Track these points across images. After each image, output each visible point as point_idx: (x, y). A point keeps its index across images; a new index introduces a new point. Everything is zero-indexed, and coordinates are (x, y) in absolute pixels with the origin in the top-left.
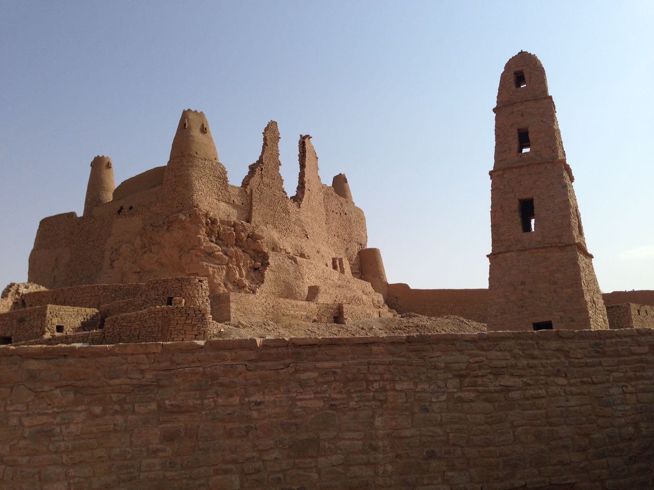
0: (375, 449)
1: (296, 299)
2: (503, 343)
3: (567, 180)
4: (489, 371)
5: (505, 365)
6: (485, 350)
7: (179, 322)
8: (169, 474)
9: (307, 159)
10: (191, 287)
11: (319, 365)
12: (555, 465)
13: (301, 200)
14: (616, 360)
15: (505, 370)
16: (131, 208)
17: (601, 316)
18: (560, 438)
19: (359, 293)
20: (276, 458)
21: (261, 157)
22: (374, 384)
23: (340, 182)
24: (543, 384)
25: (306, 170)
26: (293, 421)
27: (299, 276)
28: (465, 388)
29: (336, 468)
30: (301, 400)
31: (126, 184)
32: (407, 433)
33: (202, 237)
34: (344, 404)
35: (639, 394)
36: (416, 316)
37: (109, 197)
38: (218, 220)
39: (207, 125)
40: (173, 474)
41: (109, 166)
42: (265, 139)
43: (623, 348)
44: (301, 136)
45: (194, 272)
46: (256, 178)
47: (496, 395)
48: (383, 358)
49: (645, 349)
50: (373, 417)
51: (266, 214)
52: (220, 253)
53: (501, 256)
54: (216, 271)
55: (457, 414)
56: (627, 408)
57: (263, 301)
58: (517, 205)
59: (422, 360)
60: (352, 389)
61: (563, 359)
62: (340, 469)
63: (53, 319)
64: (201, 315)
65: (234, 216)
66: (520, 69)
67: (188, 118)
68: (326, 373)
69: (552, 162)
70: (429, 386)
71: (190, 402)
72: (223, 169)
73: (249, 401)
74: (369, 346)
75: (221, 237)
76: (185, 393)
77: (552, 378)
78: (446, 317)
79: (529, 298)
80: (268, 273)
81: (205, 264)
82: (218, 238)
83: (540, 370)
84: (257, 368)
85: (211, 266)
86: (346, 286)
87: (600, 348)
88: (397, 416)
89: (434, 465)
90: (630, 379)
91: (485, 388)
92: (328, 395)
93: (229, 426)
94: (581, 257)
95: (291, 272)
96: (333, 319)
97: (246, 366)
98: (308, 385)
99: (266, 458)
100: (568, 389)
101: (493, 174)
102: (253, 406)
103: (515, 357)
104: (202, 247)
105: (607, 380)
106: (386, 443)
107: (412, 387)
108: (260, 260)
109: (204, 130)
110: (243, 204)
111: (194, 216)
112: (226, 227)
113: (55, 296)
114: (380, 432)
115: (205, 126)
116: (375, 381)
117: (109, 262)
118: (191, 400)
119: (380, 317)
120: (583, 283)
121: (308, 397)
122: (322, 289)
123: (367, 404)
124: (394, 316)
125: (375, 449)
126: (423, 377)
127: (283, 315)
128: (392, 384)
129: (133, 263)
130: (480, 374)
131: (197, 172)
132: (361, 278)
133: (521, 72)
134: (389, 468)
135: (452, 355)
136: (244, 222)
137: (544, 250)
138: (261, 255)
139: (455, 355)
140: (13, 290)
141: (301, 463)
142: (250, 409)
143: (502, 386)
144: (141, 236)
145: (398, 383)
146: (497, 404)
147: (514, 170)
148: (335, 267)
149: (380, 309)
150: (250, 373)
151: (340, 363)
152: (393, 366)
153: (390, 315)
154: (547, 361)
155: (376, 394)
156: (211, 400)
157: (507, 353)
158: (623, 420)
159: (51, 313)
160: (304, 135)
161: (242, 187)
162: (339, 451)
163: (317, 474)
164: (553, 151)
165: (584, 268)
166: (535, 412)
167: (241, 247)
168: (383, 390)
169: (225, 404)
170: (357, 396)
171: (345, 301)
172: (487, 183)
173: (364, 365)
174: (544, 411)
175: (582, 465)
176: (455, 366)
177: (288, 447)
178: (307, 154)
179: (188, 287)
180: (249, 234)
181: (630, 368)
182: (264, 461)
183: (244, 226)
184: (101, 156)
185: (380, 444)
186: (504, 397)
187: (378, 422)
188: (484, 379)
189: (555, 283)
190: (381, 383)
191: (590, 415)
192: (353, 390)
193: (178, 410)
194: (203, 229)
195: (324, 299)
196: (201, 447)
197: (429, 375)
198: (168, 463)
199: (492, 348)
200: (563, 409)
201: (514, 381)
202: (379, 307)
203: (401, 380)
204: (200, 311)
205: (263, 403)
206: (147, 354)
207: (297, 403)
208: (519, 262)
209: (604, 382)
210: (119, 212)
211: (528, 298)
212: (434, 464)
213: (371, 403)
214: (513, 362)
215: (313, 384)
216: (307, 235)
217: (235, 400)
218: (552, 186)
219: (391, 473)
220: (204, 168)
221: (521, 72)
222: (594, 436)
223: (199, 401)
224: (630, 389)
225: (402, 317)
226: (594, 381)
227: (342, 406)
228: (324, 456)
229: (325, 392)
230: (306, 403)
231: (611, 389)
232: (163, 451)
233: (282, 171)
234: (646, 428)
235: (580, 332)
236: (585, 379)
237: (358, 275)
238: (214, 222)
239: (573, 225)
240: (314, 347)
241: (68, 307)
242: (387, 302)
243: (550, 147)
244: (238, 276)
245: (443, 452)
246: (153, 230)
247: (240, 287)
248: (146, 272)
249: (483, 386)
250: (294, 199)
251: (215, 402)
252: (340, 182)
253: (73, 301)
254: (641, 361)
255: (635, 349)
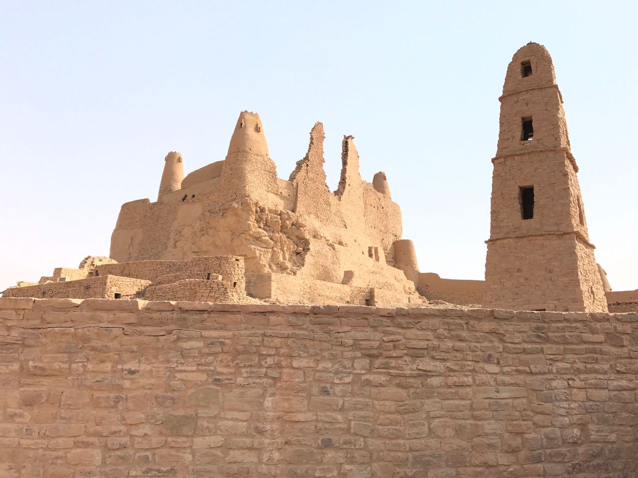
0: (261, 432)
1: (332, 281)
2: (426, 321)
3: (570, 168)
4: (405, 352)
5: (426, 347)
6: (403, 328)
7: (204, 294)
8: (25, 442)
9: (349, 157)
10: (228, 265)
11: (205, 333)
12: (477, 466)
13: (342, 194)
14: (562, 347)
15: (425, 352)
16: (194, 196)
17: (600, 307)
18: (486, 435)
19: (392, 281)
20: (145, 435)
21: (307, 154)
22: (268, 358)
23: (379, 181)
24: (470, 371)
25: (347, 167)
26: (169, 394)
27: (336, 261)
28: (375, 370)
29: (213, 451)
30: (181, 371)
31: (191, 176)
32: (301, 417)
33: (252, 223)
34: (231, 380)
35: (589, 390)
36: (444, 303)
37: (178, 186)
38: (267, 209)
39: (261, 124)
40: (29, 442)
41: (179, 160)
42: (312, 138)
43: (571, 334)
44: (345, 136)
45: (243, 254)
46: (302, 172)
47: (412, 380)
48: (281, 330)
49: (601, 338)
50: (263, 396)
51: (309, 205)
52: (267, 238)
53: (498, 242)
54: (262, 253)
55: (362, 400)
56: (572, 406)
57: (301, 282)
58: (518, 192)
59: (326, 335)
60: (241, 363)
61: (496, 344)
62: (218, 453)
63: (112, 287)
64: (223, 289)
65: (281, 206)
66: (527, 59)
67: (244, 118)
68: (212, 344)
69: (554, 150)
70: (333, 364)
71: (56, 366)
72: (273, 164)
73: (122, 369)
74: (267, 315)
75: (268, 224)
76: (51, 355)
77: (481, 364)
78: (471, 305)
79: (524, 285)
80: (308, 258)
81: (253, 247)
82: (266, 225)
83: (467, 355)
84: (135, 333)
85: (258, 249)
86: (379, 272)
87: (542, 333)
88: (291, 397)
89: (330, 455)
90: (578, 371)
91: (399, 372)
92: (213, 368)
93: (97, 394)
94: (580, 248)
95: (329, 257)
96: (364, 302)
97: (124, 329)
98: (191, 355)
99: (134, 433)
100: (500, 378)
101: (496, 161)
102: (125, 375)
103: (438, 338)
104: (251, 232)
105: (549, 371)
106: (275, 426)
107: (312, 365)
108: (302, 246)
109: (258, 129)
110: (289, 195)
111: (246, 205)
112: (273, 215)
113: (122, 269)
114: (268, 413)
115: (259, 126)
116: (270, 355)
117: (174, 242)
118: (57, 363)
119: (409, 302)
120: (579, 273)
121: (189, 368)
122: (356, 274)
123: (258, 381)
124: (424, 302)
125: (261, 432)
126: (326, 354)
127: (319, 295)
128: (289, 361)
129: (192, 244)
130: (394, 355)
131: (250, 166)
132: (394, 266)
133: (529, 62)
134: (276, 455)
135: (363, 331)
136: (289, 212)
137: (542, 238)
138: (302, 241)
139: (367, 332)
140: (89, 262)
141: (173, 441)
142: (122, 377)
143: (419, 370)
144: (201, 221)
145: (295, 359)
146: (412, 390)
147: (516, 158)
148: (370, 255)
149: (410, 295)
150: (127, 338)
151: (231, 333)
152: (292, 339)
153: (420, 301)
154: (476, 344)
155: (269, 371)
156: (81, 364)
157: (429, 333)
158: (566, 419)
159: (110, 282)
160: (347, 135)
161: (289, 180)
162: (219, 432)
163: (191, 456)
164: (556, 139)
165: (582, 257)
166: (457, 402)
167: (286, 233)
168: (278, 366)
169: (95, 370)
170: (247, 372)
171: (377, 286)
172: (489, 169)
173: (258, 337)
174: (468, 402)
175: (511, 469)
176: (364, 344)
177: (160, 422)
178: (349, 153)
179: (226, 265)
180: (293, 222)
181: (579, 359)
182: (131, 436)
183: (290, 215)
184: (173, 152)
185: (268, 427)
186: (422, 383)
187: (268, 402)
188: (399, 362)
189: (551, 271)
190: (276, 358)
191: (525, 410)
192: (242, 365)
193: (42, 373)
194: (253, 216)
195: (358, 282)
196: (63, 415)
197: (334, 352)
198: (24, 430)
199: (412, 326)
200: (492, 401)
201: (434, 366)
202: (410, 293)
203: (299, 356)
204: (223, 285)
205: (138, 371)
206: (16, 310)
207: (176, 375)
208: (516, 249)
209: (545, 373)
210: (184, 199)
211: (523, 285)
212: (330, 454)
213: (262, 381)
214: (436, 343)
215: (197, 355)
216: (345, 225)
217: (107, 367)
218: (553, 174)
219: (277, 461)
220: (256, 163)
221: (529, 62)
222: (526, 436)
223: (66, 365)
224: (578, 383)
225: (430, 303)
226: (533, 371)
227: (227, 381)
228: (202, 436)
229: (209, 364)
230: (186, 376)
231: (553, 381)
232: (21, 416)
233: (325, 167)
234: (597, 431)
235: (520, 313)
236: (521, 368)
237: (393, 264)
238: (262, 210)
239: (573, 213)
240: (203, 313)
241: (126, 278)
242: (418, 289)
243: (553, 135)
244: (281, 259)
245: (341, 441)
246: (210, 215)
247: (282, 268)
248: (203, 252)
249: (397, 368)
250: (336, 193)
251: (84, 366)
252: (379, 181)
253: (136, 273)
254: (594, 351)
255: (588, 336)
